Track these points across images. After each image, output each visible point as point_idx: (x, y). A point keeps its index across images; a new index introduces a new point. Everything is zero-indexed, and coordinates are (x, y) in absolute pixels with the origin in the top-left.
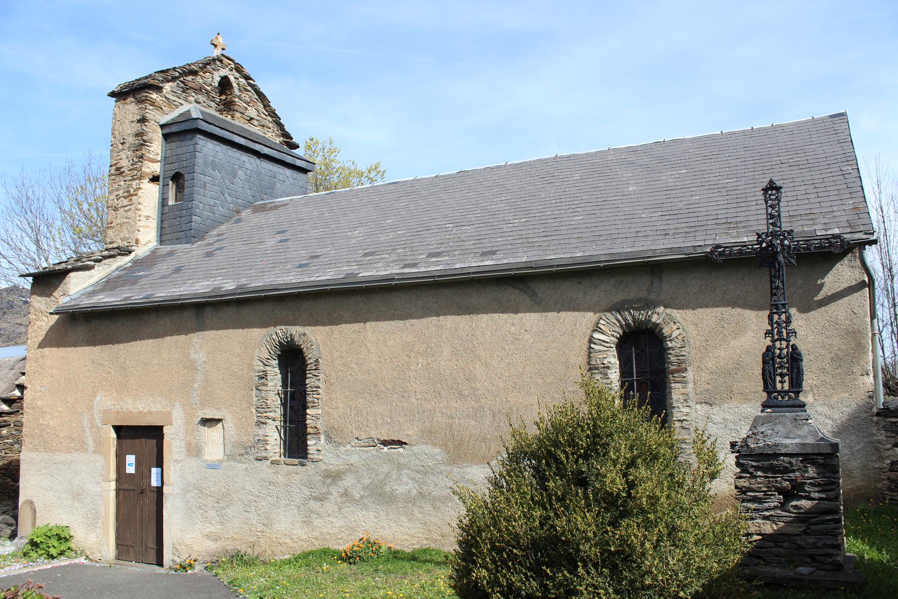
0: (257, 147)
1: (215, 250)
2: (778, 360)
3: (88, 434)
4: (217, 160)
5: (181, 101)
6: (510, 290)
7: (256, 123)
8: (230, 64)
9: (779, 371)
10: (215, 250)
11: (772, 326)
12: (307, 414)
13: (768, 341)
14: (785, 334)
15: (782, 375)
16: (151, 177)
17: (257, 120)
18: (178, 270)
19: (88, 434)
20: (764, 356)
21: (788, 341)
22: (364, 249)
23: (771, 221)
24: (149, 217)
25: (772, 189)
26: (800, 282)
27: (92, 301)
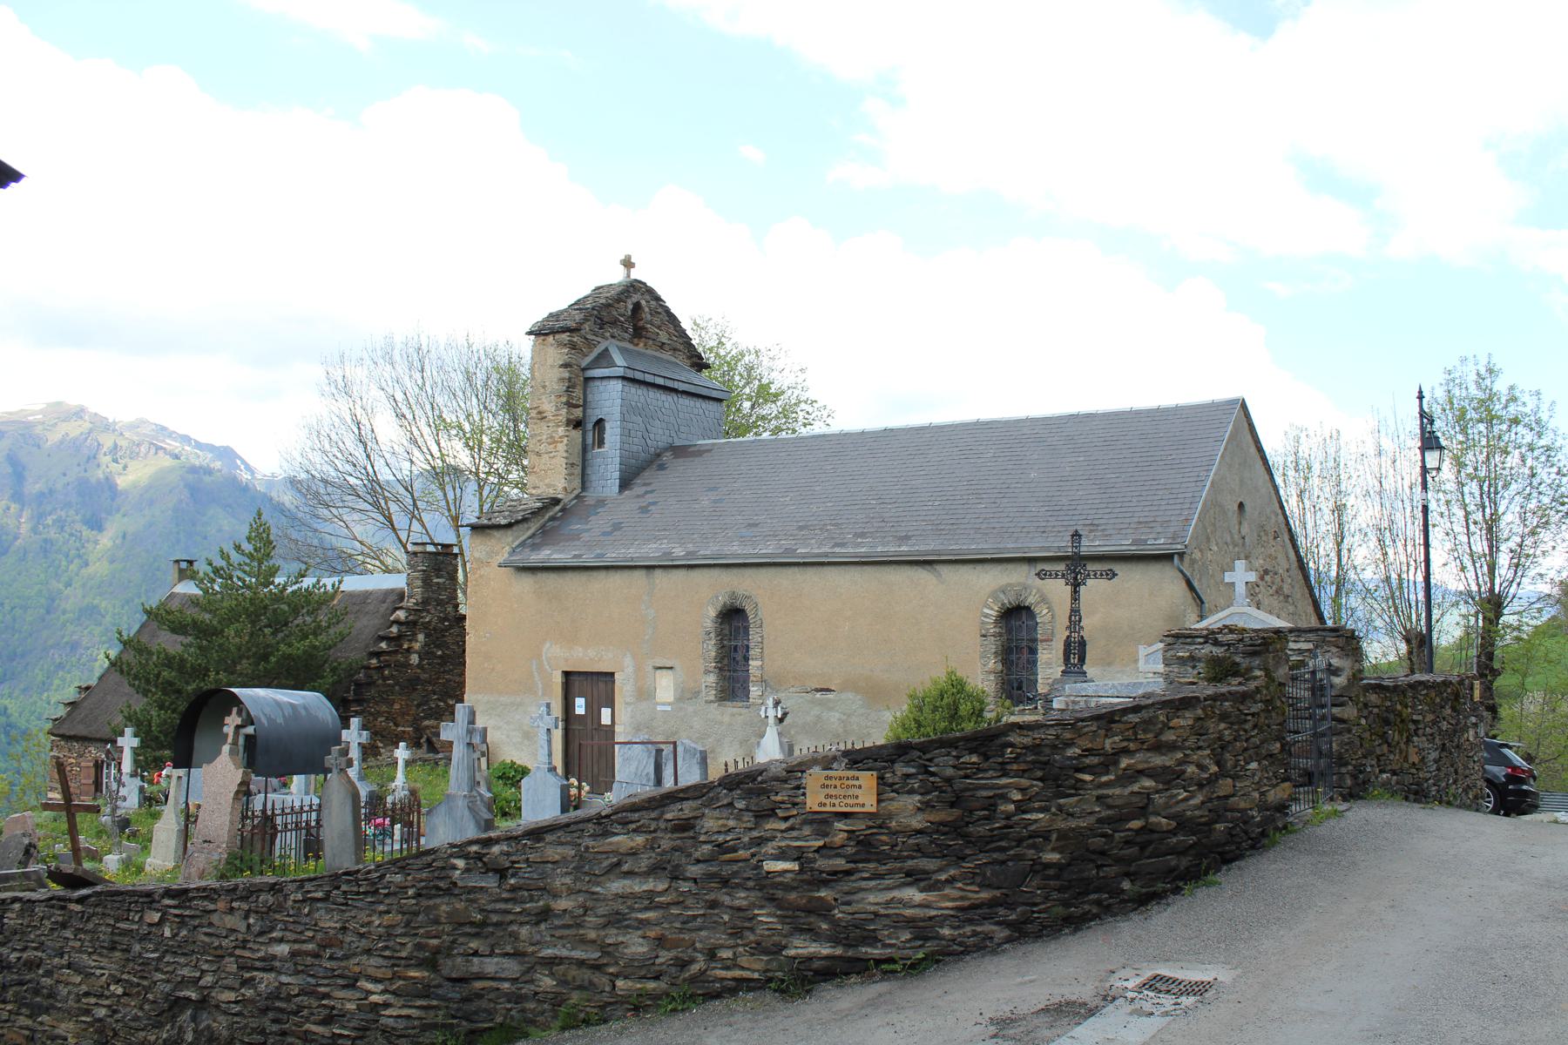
0: (676, 385)
3: (537, 678)
5: (599, 339)
13: (1067, 633)
15: (1074, 654)
18: (617, 527)
20: (1065, 641)
21: (1079, 633)
22: (797, 522)
27: (540, 557)
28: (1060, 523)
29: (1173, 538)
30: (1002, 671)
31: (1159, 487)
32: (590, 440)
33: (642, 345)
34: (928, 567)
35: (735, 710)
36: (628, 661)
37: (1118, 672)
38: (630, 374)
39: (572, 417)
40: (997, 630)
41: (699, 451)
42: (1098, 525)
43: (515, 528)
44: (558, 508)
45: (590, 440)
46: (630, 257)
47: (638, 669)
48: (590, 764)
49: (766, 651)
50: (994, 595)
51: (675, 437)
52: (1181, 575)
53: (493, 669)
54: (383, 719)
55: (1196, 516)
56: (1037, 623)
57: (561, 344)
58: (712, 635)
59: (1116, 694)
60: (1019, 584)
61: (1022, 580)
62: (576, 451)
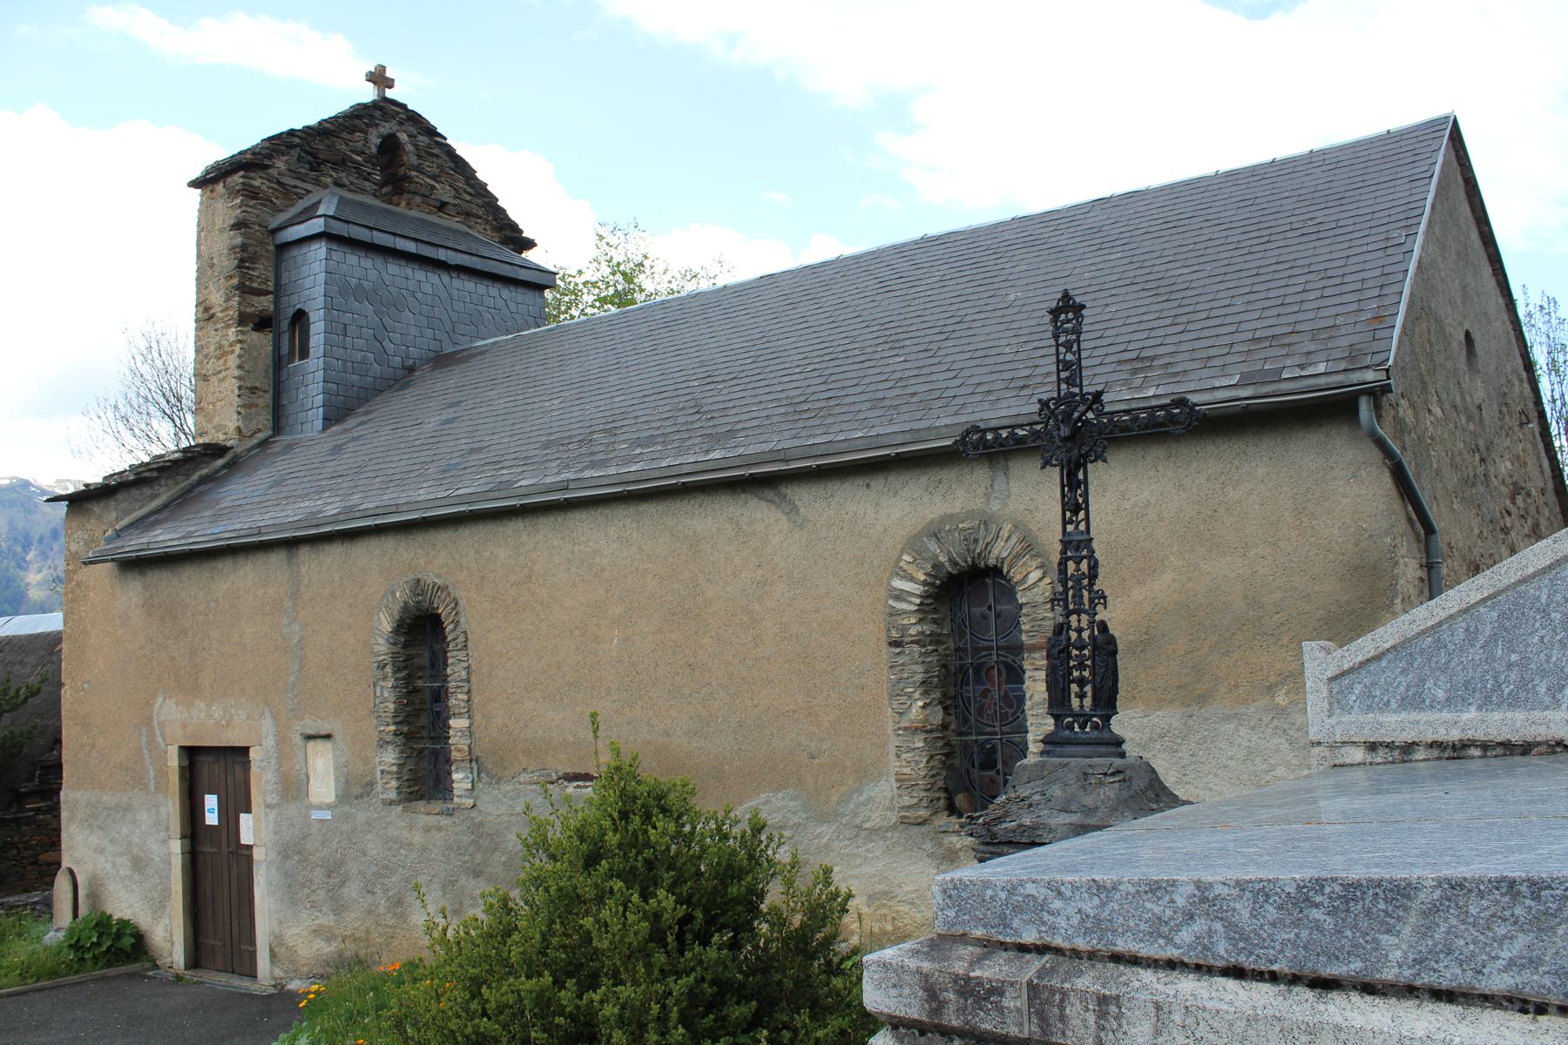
0: (442, 255)
1: (347, 442)
2: (1075, 652)
4: (365, 283)
5: (309, 187)
6: (753, 502)
7: (451, 210)
8: (398, 113)
9: (1076, 674)
10: (347, 442)
11: (1065, 585)
12: (449, 727)
13: (1057, 616)
14: (1086, 601)
15: (1081, 682)
16: (257, 320)
17: (455, 205)
23: (1063, 375)
24: (256, 388)
25: (1067, 309)
26: (1261, 471)
29: (1351, 358)
30: (944, 727)
31: (1295, 272)
32: (285, 349)
33: (403, 204)
34: (770, 494)
36: (267, 725)
37: (1227, 718)
38: (340, 229)
39: (249, 310)
40: (927, 629)
42: (1153, 358)
43: (120, 496)
45: (285, 349)
47: (282, 740)
48: (227, 919)
49: (476, 699)
50: (914, 545)
52: (1376, 454)
53: (93, 746)
55: (1403, 308)
57: (232, 193)
58: (389, 669)
59: (1223, 951)
60: (970, 515)
61: (977, 504)
62: (261, 366)
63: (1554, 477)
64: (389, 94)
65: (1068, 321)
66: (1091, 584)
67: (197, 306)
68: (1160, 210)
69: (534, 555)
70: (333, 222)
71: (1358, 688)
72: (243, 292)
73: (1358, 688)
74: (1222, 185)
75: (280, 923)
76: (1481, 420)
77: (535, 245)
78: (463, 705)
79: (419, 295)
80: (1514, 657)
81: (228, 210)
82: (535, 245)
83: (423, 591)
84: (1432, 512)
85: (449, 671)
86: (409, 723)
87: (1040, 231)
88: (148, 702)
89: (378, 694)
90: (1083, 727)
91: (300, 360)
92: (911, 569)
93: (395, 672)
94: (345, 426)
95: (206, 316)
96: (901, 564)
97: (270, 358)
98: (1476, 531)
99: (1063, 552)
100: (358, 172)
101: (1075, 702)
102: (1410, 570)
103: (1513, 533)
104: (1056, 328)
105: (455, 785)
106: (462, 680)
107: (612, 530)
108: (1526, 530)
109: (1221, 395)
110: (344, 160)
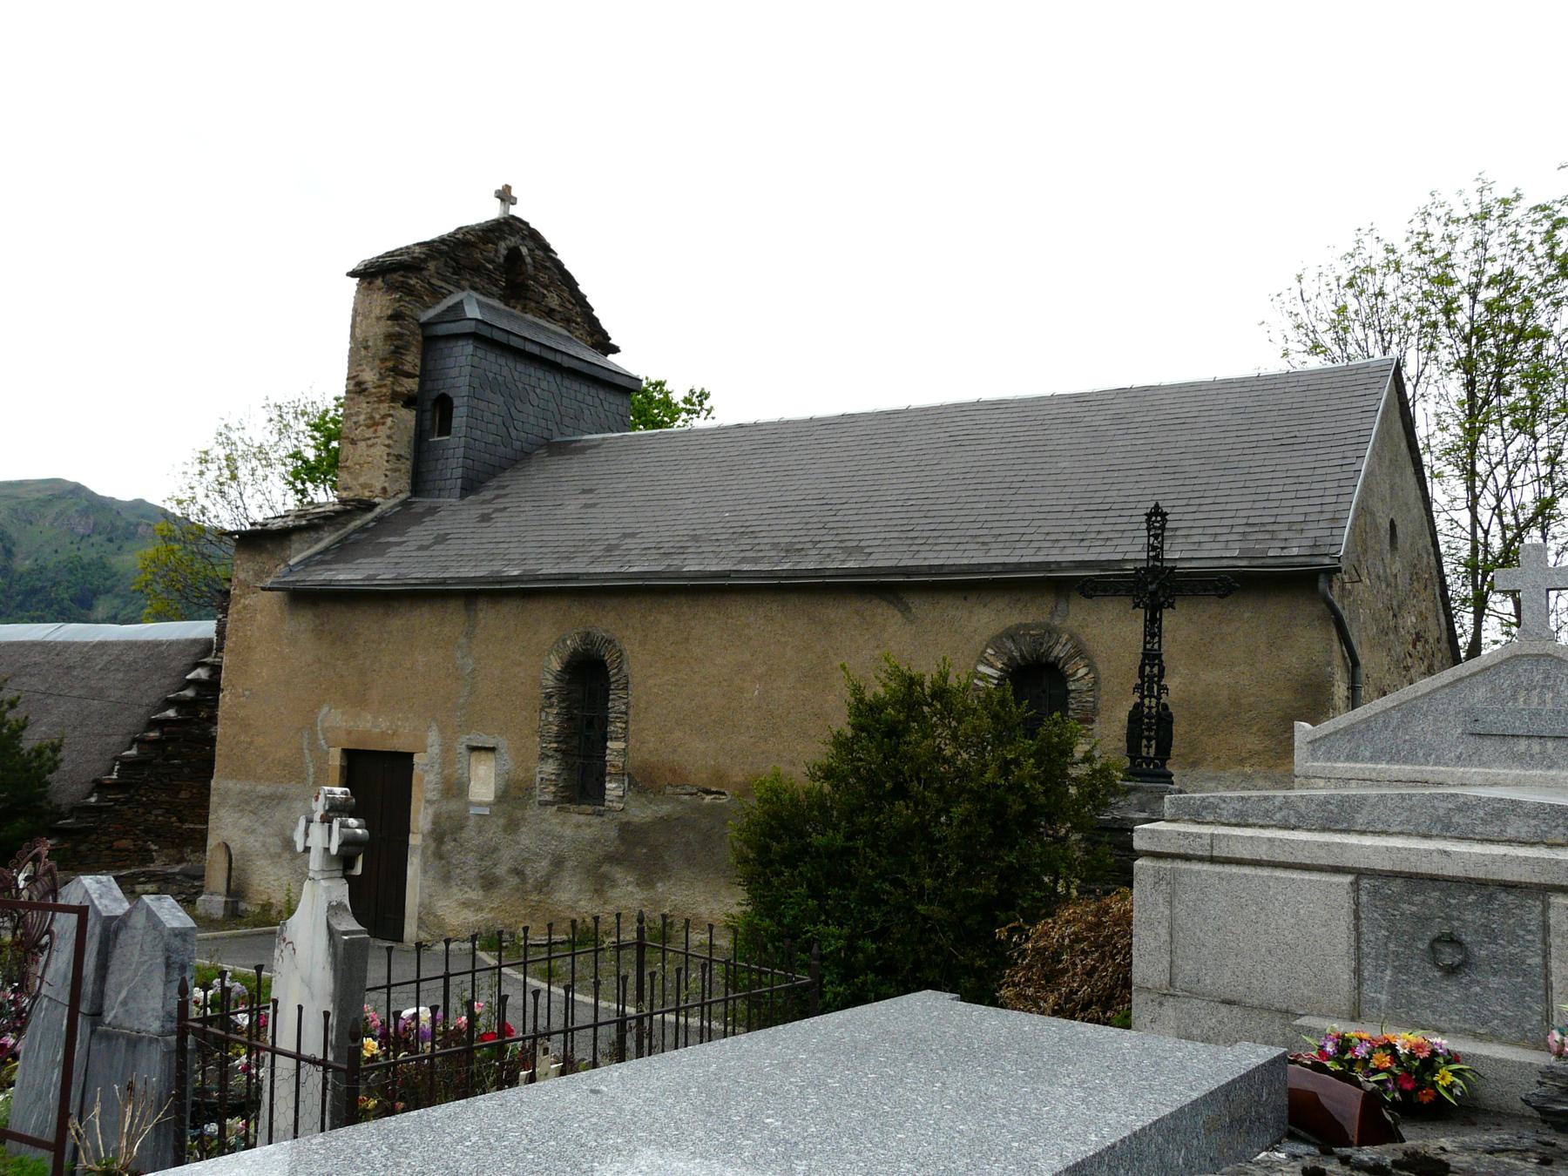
1: (493, 512)
2: (1146, 720)
4: (499, 378)
5: (451, 288)
8: (522, 229)
9: (1146, 733)
11: (1142, 680)
12: (607, 748)
13: (1136, 698)
15: (1149, 739)
16: (405, 399)
17: (559, 312)
19: (308, 758)
21: (1159, 698)
23: (1151, 554)
26: (1247, 615)
28: (1109, 528)
35: (582, 818)
36: (433, 737)
39: (399, 389)
41: (583, 446)
44: (370, 516)
45: (427, 424)
46: (507, 188)
47: (446, 749)
49: (632, 728)
50: (996, 642)
51: (556, 432)
54: (159, 812)
56: (1068, 692)
57: (391, 288)
58: (554, 700)
60: (1038, 626)
61: (1044, 618)
63: (1448, 629)
64: (514, 211)
65: (1158, 522)
66: (1160, 681)
67: (348, 379)
68: (1173, 406)
69: (692, 623)
70: (481, 326)
71: (1323, 749)
72: (397, 374)
73: (1323, 749)
74: (1219, 391)
75: (431, 896)
76: (1396, 586)
77: (619, 351)
78: (620, 731)
79: (538, 391)
80: (1407, 737)
81: (382, 302)
82: (619, 351)
83: (592, 641)
84: (1358, 651)
85: (610, 705)
86: (567, 743)
87: (1076, 410)
88: (312, 711)
89: (543, 718)
90: (1148, 765)
91: (439, 436)
92: (992, 659)
93: (559, 702)
94: (481, 497)
95: (358, 389)
96: (986, 655)
97: (413, 432)
98: (1387, 667)
99: (1143, 660)
100: (489, 279)
101: (1144, 751)
102: (1341, 690)
103: (1412, 671)
104: (1149, 525)
105: (607, 792)
106: (621, 713)
107: (760, 611)
108: (1423, 669)
109: (1225, 563)
110: (478, 267)
